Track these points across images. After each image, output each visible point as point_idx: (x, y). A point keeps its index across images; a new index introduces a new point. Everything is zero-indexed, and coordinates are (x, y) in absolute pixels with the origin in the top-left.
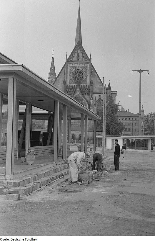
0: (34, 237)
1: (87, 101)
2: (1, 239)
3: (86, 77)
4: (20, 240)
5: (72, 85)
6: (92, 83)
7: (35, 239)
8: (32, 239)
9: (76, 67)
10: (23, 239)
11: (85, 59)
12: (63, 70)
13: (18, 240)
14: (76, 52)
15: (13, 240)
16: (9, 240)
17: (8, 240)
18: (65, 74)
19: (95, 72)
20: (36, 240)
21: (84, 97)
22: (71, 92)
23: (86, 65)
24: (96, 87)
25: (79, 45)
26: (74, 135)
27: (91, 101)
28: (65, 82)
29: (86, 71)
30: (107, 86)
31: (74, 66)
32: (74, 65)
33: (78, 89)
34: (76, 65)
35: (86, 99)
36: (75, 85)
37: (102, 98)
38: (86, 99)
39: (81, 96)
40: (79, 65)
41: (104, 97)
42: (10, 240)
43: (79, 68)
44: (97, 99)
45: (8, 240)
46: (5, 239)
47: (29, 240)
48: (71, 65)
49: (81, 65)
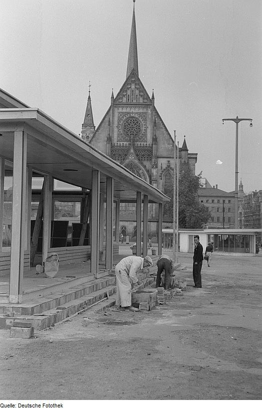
0: (58, 402)
1: (148, 171)
2: (2, 405)
3: (146, 130)
4: (34, 406)
5: (122, 143)
6: (155, 140)
7: (59, 405)
8: (54, 405)
9: (128, 113)
10: (40, 405)
11: (144, 99)
12: (107, 119)
13: (31, 406)
14: (128, 88)
15: (23, 406)
16: (15, 406)
17: (13, 406)
18: (109, 125)
19: (161, 122)
20: (60, 406)
21: (142, 164)
22: (120, 155)
23: (145, 110)
24: (163, 148)
25: (133, 75)
26: (125, 228)
27: (154, 171)
28: (109, 139)
29: (145, 120)
30: (181, 146)
31: (125, 111)
32: (124, 110)
33: (132, 151)
34: (128, 110)
35: (145, 167)
36: (127, 143)
37: (172, 166)
38: (145, 167)
39: (136, 161)
40: (133, 110)
41: (175, 163)
42: (17, 406)
43: (133, 115)
44: (164, 167)
45: (13, 406)
46: (9, 405)
47: (49, 406)
48: (120, 110)
49: (137, 110)
